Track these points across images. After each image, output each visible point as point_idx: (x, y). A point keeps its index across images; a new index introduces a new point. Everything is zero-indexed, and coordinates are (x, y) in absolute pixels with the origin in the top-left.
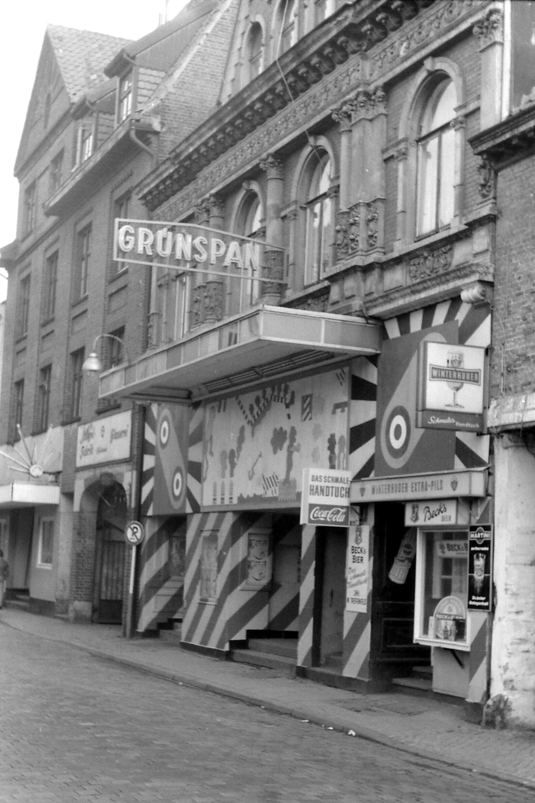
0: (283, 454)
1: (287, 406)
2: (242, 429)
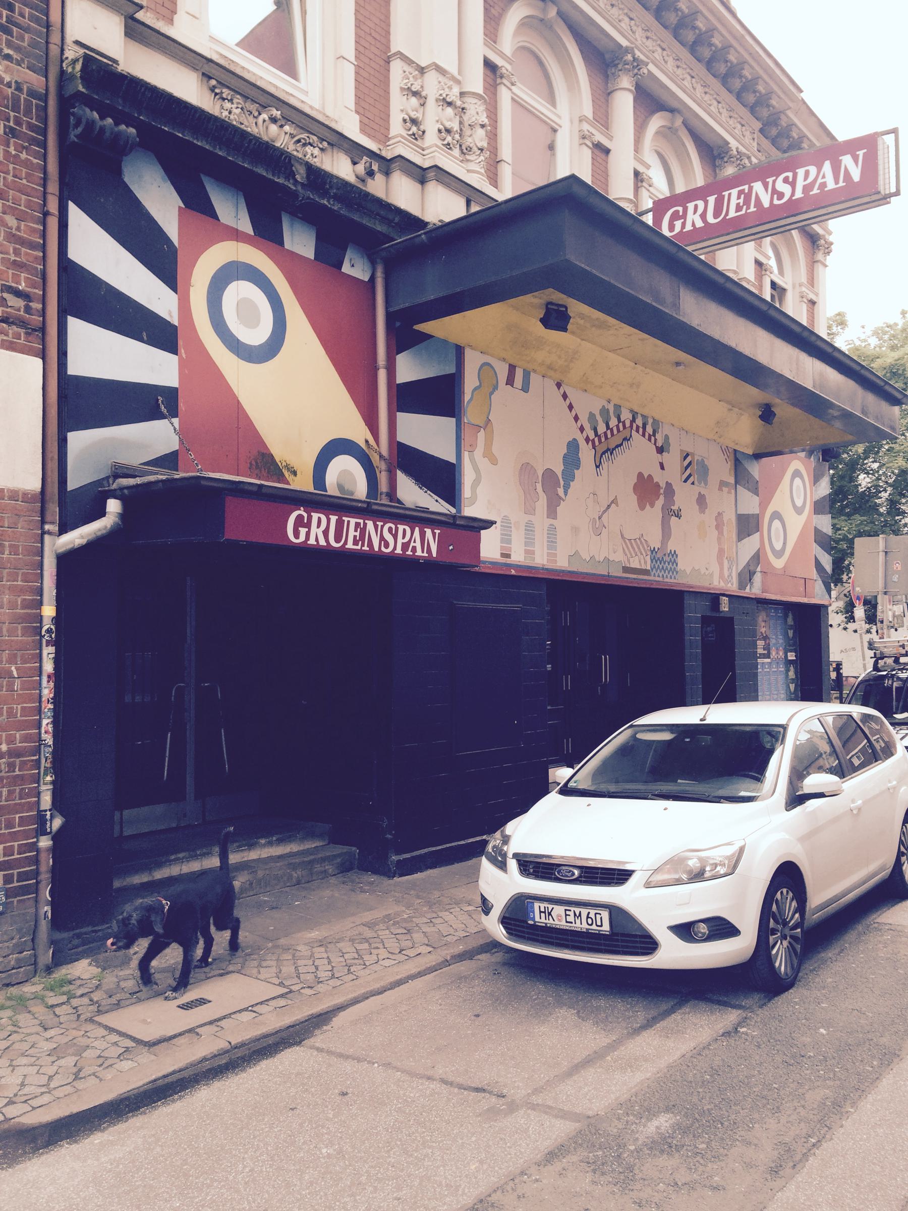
0: (655, 512)
1: (660, 450)
2: (573, 446)
